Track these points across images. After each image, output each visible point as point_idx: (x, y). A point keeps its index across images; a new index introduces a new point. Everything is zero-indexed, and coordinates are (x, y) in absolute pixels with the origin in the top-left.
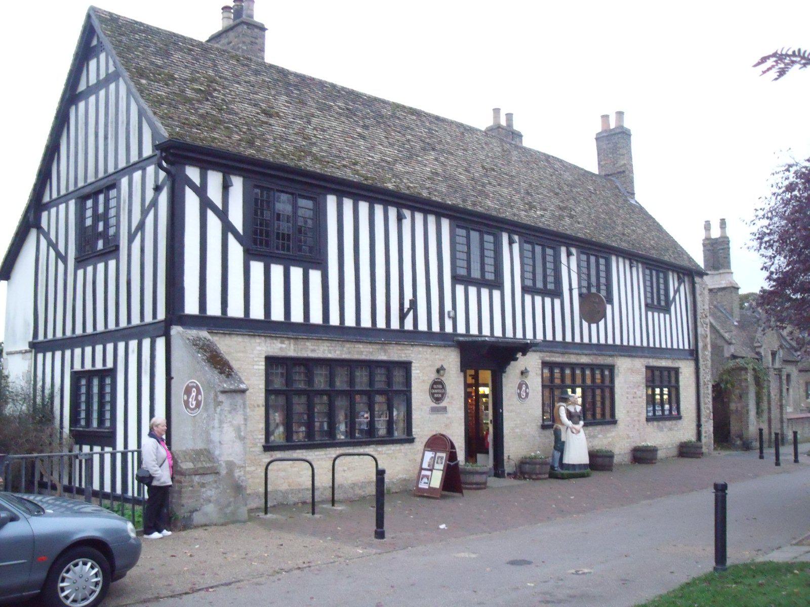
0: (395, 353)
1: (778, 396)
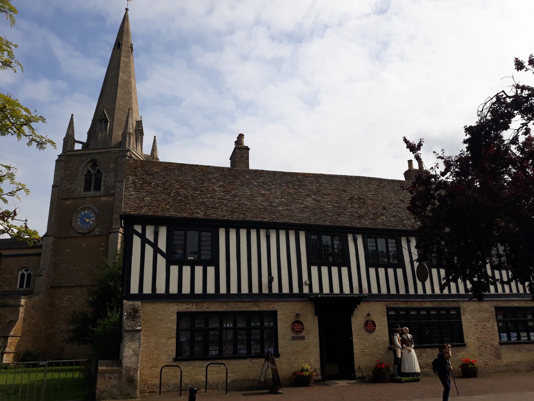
0: (265, 307)
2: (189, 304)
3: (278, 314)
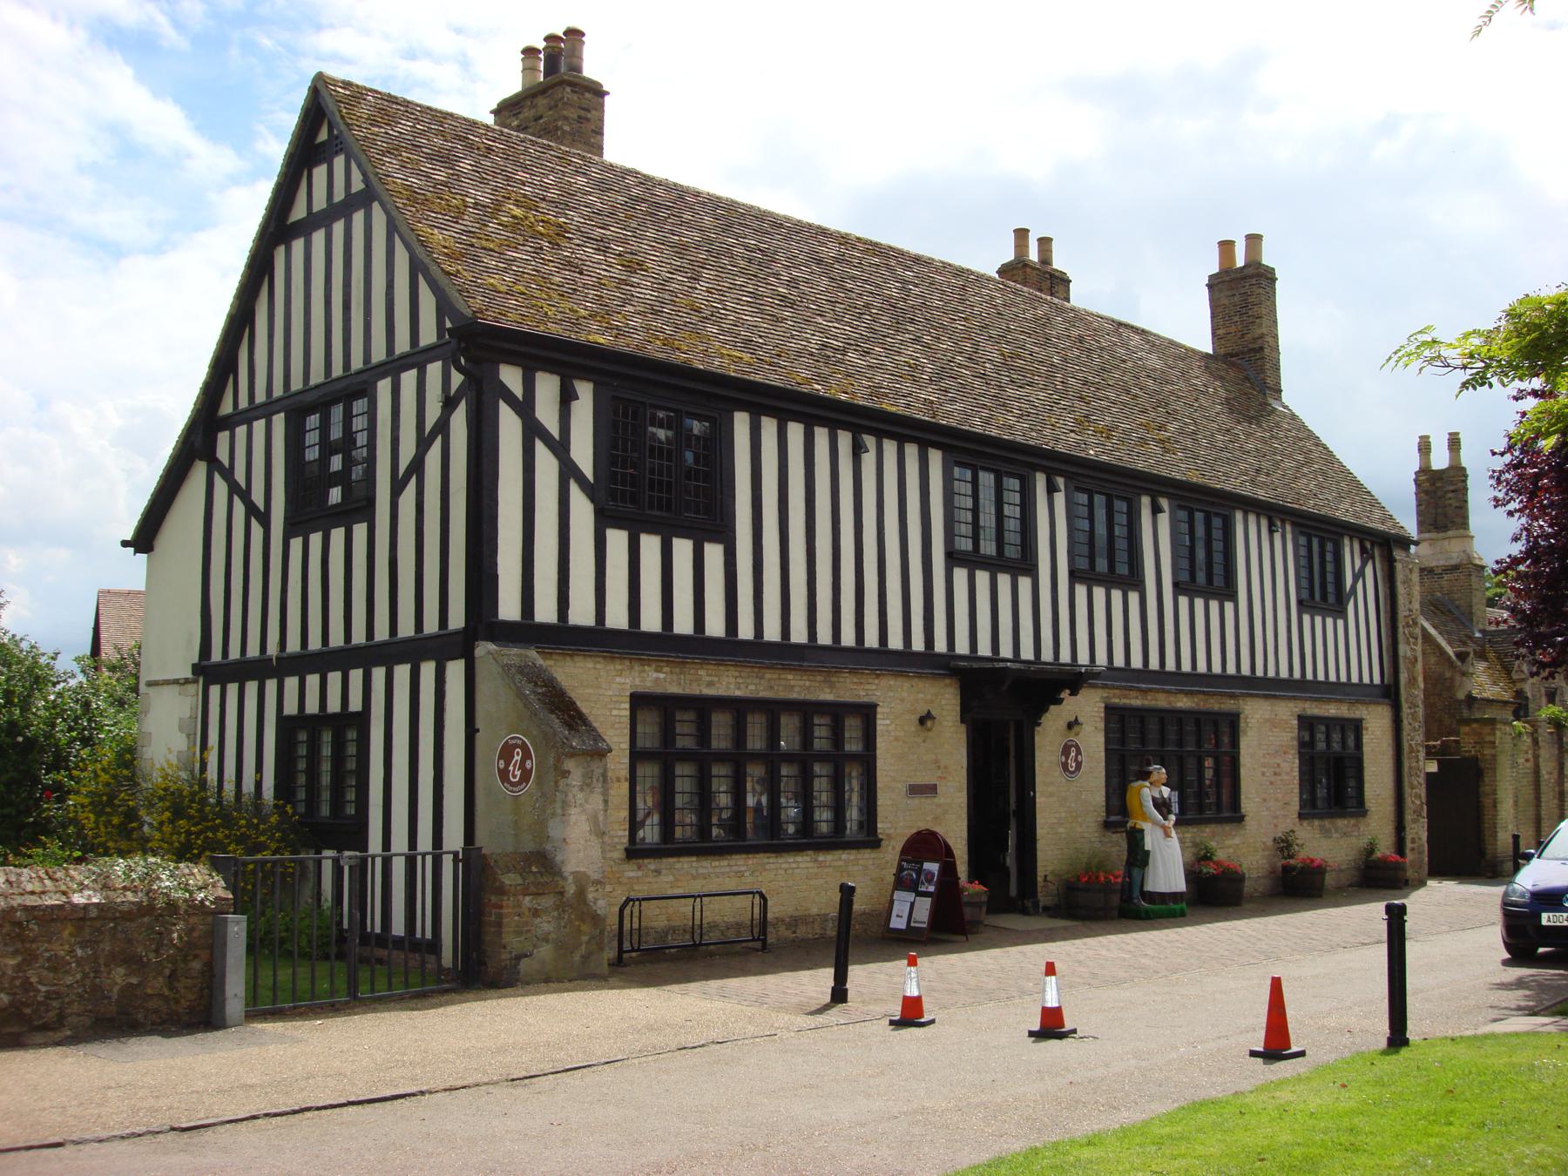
0: (849, 688)
1: (1555, 776)
2: (662, 667)
3: (879, 716)
